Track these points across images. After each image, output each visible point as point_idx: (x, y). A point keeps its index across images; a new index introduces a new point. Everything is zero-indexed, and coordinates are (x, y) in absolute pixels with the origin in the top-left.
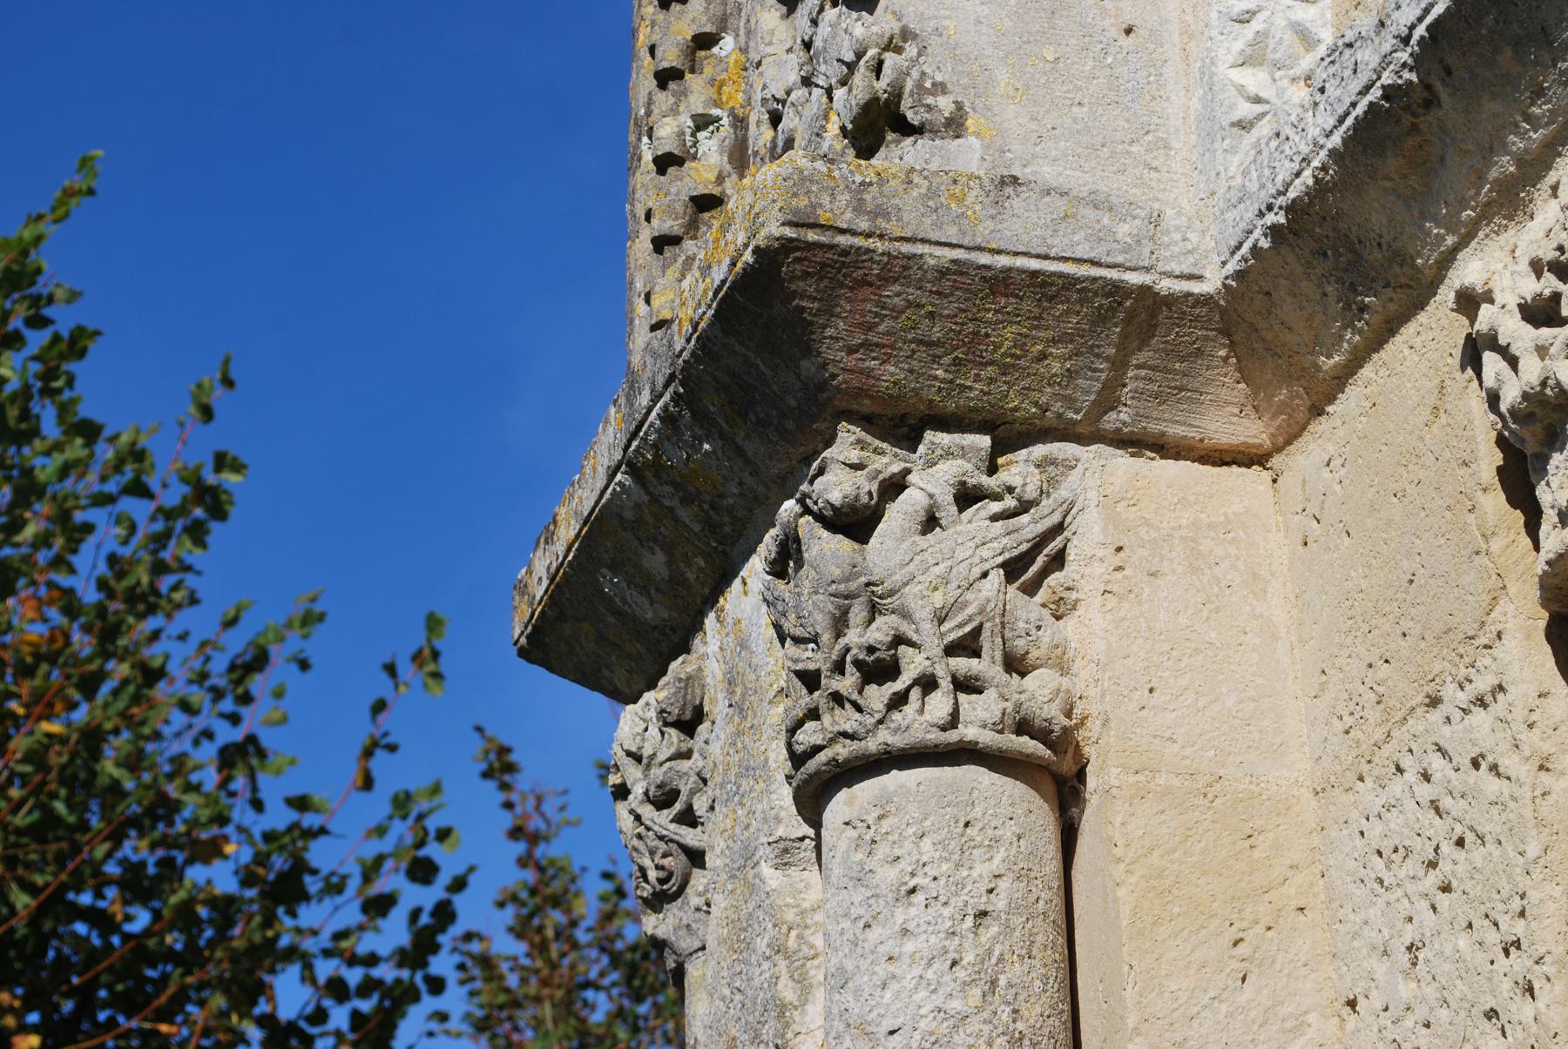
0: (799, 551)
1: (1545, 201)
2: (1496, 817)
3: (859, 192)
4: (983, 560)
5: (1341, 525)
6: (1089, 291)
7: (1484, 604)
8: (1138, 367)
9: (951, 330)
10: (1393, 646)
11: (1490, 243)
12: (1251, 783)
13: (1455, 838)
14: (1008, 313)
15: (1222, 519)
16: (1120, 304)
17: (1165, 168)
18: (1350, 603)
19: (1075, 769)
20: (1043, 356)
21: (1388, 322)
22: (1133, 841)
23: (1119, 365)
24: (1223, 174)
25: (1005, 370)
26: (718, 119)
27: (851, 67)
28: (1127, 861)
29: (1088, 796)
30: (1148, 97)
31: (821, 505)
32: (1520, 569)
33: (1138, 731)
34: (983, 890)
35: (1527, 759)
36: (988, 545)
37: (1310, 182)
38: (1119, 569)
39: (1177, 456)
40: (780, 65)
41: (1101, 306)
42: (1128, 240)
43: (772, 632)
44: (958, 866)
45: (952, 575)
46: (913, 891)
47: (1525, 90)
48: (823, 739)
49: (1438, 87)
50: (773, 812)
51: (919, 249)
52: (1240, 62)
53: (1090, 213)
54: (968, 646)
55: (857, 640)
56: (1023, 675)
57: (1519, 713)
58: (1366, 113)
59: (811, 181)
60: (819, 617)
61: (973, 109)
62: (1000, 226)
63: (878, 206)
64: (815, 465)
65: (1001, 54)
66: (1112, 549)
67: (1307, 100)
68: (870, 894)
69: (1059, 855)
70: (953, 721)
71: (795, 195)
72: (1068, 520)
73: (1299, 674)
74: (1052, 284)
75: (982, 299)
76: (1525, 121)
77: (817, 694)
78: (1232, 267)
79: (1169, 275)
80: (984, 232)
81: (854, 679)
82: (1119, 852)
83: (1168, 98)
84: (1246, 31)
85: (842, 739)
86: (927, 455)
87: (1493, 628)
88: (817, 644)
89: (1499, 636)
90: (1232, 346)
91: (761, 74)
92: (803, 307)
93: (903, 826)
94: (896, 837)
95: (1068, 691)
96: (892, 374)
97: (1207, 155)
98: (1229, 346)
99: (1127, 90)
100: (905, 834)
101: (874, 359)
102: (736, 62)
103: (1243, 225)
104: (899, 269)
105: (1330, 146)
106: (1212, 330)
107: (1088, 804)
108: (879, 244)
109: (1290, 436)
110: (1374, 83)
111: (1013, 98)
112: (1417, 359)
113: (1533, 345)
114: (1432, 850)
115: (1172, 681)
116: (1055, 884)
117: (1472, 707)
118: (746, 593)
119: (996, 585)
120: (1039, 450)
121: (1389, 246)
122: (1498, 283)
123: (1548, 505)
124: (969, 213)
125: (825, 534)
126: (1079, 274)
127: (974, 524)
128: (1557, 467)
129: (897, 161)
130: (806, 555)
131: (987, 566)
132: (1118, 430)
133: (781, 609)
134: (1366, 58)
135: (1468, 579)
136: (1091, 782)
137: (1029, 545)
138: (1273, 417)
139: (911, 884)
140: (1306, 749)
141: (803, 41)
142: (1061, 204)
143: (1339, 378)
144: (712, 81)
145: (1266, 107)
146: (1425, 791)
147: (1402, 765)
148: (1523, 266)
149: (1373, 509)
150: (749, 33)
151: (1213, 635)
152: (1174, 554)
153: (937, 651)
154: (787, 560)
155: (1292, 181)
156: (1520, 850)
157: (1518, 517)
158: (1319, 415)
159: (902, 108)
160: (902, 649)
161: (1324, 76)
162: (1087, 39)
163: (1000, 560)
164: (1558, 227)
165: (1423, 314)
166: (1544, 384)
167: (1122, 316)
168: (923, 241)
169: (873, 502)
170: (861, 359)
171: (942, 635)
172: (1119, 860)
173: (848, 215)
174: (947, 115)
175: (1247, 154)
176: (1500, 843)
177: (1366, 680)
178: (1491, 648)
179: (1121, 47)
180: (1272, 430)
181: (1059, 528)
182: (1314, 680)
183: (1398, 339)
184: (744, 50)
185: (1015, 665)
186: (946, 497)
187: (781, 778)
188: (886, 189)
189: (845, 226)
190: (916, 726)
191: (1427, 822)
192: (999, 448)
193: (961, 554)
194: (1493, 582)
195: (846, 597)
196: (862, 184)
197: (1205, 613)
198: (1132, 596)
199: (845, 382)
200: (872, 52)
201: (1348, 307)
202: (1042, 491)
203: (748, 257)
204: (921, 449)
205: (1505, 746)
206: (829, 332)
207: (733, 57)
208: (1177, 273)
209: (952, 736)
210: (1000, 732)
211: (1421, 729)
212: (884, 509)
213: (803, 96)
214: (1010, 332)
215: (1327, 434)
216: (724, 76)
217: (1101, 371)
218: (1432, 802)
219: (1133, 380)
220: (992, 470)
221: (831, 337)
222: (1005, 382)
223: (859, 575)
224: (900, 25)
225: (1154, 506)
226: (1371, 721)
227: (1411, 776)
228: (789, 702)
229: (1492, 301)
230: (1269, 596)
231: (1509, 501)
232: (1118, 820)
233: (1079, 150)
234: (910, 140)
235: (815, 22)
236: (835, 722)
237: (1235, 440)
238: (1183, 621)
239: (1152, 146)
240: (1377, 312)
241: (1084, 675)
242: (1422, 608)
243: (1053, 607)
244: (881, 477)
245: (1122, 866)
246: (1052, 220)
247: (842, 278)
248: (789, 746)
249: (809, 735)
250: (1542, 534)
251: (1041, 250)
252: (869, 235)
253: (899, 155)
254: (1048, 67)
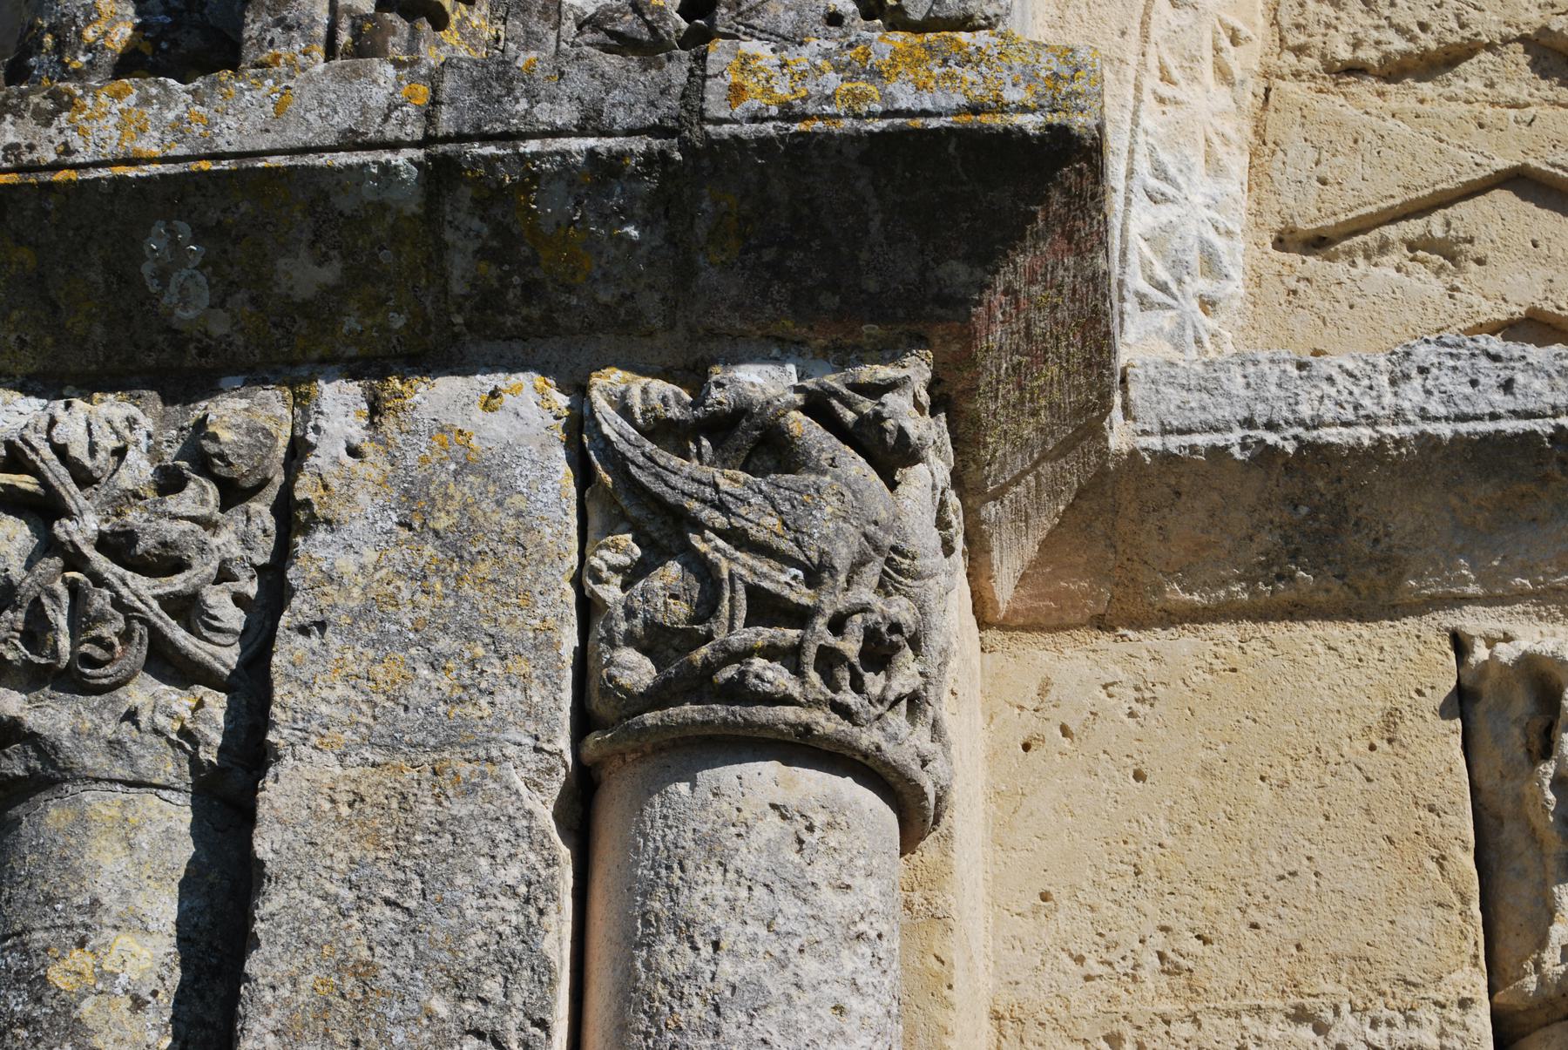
11: (1525, 622)
52: (1147, 236)
58: (1516, 435)
143: (1170, 614)
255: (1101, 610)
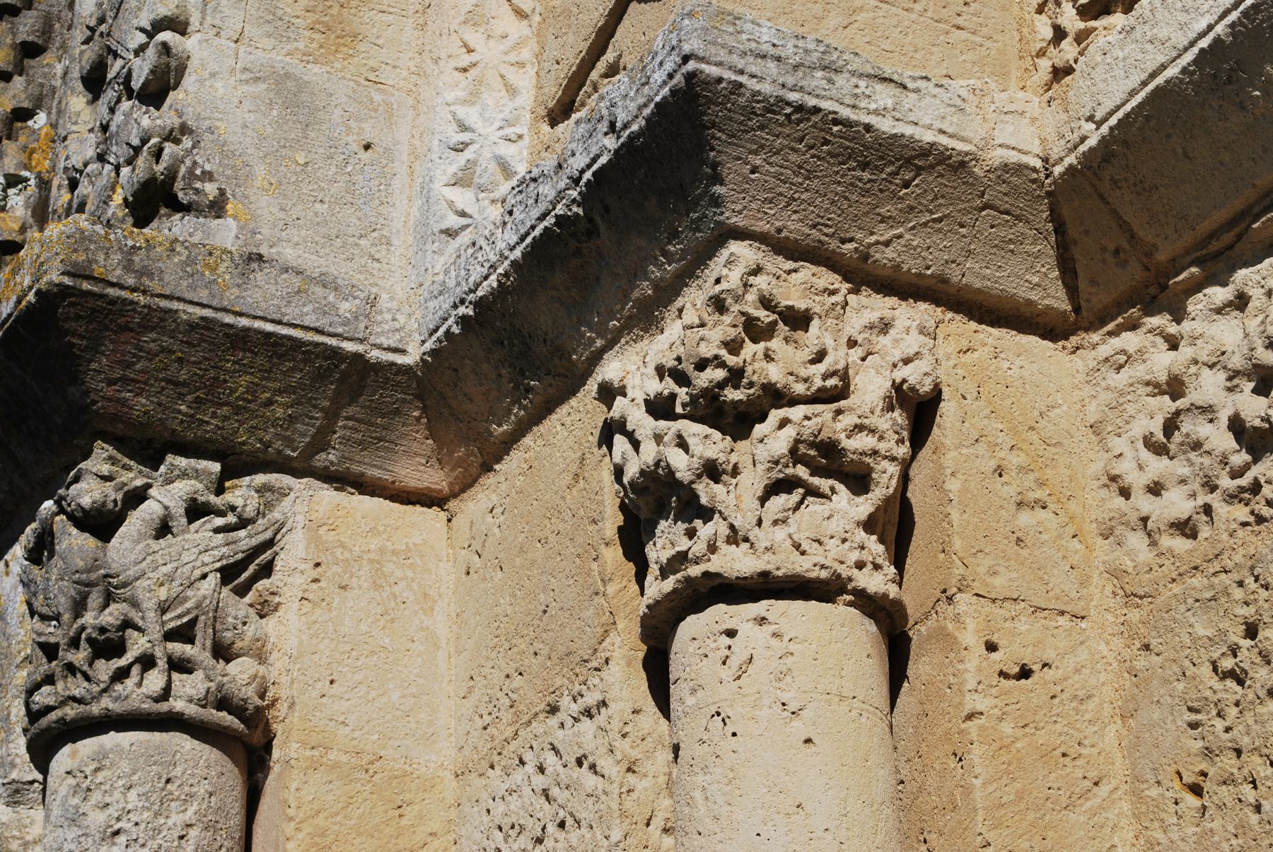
0: (53, 544)
1: (673, 320)
2: (591, 807)
3: (130, 254)
4: (204, 564)
5: (497, 561)
6: (313, 353)
7: (598, 635)
8: (347, 418)
9: (196, 374)
10: (526, 662)
11: (629, 349)
12: (405, 763)
13: (558, 821)
14: (244, 365)
15: (404, 547)
16: (336, 366)
17: (386, 261)
18: (497, 624)
19: (263, 741)
20: (270, 402)
21: (547, 402)
22: (303, 804)
23: (332, 416)
24: (430, 270)
25: (237, 410)
26: (27, 180)
27: (137, 150)
28: (297, 820)
29: (272, 764)
30: (377, 202)
31: (73, 507)
32: (628, 609)
33: (318, 714)
34: (176, 836)
35: (619, 762)
36: (210, 552)
37: (495, 285)
38: (316, 581)
39: (373, 494)
40: (82, 141)
41: (321, 367)
42: (348, 315)
43: (25, 608)
44: (157, 814)
45: (177, 575)
46: (117, 833)
47: (664, 232)
48: (56, 701)
49: (599, 221)
50: (9, 759)
51: (175, 305)
53: (319, 291)
54: (184, 634)
55: (92, 621)
56: (228, 661)
57: (616, 725)
58: (541, 234)
59: (90, 241)
60: (63, 600)
61: (234, 196)
62: (244, 294)
63: (145, 267)
64: (72, 474)
65: (261, 154)
66: (311, 564)
67: (498, 221)
68: (81, 833)
69: (243, 812)
70: (166, 694)
71: (75, 251)
72: (278, 537)
73: (453, 678)
74: (282, 345)
75: (223, 351)
76: (662, 256)
77: (54, 663)
78: (429, 345)
79: (379, 347)
80: (230, 296)
81: (86, 653)
82: (291, 812)
83: (394, 204)
84: (459, 158)
85: (71, 703)
86: (166, 474)
87: (603, 654)
88: (59, 622)
89: (607, 661)
90: (424, 409)
91: (66, 147)
92: (74, 344)
93: (115, 779)
94: (108, 787)
95: (263, 677)
96: (143, 405)
97: (420, 253)
98: (422, 409)
99: (361, 194)
100: (115, 785)
101: (129, 391)
102: (47, 134)
103: (440, 313)
104: (158, 320)
105: (512, 257)
106: (409, 394)
107: (271, 771)
108: (141, 298)
109: (464, 486)
110: (550, 212)
111: (267, 190)
112: (566, 434)
113: (652, 433)
114: (540, 829)
115: (349, 676)
116: (237, 835)
117: (581, 717)
118: (7, 574)
119: (213, 586)
120: (260, 479)
121: (552, 343)
122: (631, 381)
123: (653, 560)
124: (220, 280)
125: (74, 531)
126: (306, 339)
127: (200, 534)
128: (663, 532)
129: (166, 231)
130: (57, 547)
131: (207, 569)
132: (326, 468)
133: (33, 589)
134: (546, 192)
135: (588, 614)
136: (276, 753)
137: (244, 555)
138: (453, 469)
139: (116, 827)
140: (453, 739)
141: (101, 124)
142: (296, 281)
144: (24, 149)
145: (468, 221)
146: (539, 781)
147: (524, 759)
148: (651, 370)
149: (522, 550)
150: (59, 112)
151: (387, 641)
152: (362, 573)
153: (157, 636)
154: (41, 551)
155: (481, 282)
156: (606, 834)
157: (631, 568)
158: (489, 471)
159: (175, 189)
160: (129, 631)
161: (513, 202)
162: (332, 150)
163: (218, 565)
164: (678, 342)
165: (574, 399)
166: (657, 464)
167: (337, 376)
168: (179, 299)
169: (117, 509)
170: (118, 391)
171: (163, 623)
172: (291, 819)
173: (118, 272)
174: (211, 198)
175: (450, 256)
176: (592, 828)
177: (504, 688)
178: (600, 670)
179: (360, 160)
180: (450, 479)
181: (270, 543)
182: (464, 684)
183: (554, 416)
184: (54, 126)
185: (223, 652)
186: (178, 510)
187: (19, 730)
188: (152, 254)
189: (115, 281)
190: (134, 696)
191: (538, 807)
192: (227, 474)
193: (186, 557)
194: (606, 618)
195: (87, 585)
196: (133, 247)
197: (382, 623)
198: (324, 604)
199: (103, 407)
200: (154, 141)
201: (516, 387)
202: (258, 513)
203: (31, 297)
204: (162, 469)
205: (603, 750)
206: (94, 366)
207: (45, 130)
208: (385, 346)
209: (163, 707)
210: (204, 707)
211: (541, 731)
212: (126, 515)
213: (97, 169)
214: (244, 380)
215: (493, 487)
216: (35, 145)
217: (317, 419)
218: (544, 790)
219: (342, 429)
220: (220, 491)
221: (95, 370)
222: (236, 421)
223: (99, 568)
224: (180, 121)
225: (349, 532)
226: (504, 721)
227: (530, 768)
228: (31, 668)
229: (625, 395)
230: (436, 612)
231: (625, 554)
232: (294, 785)
233: (317, 239)
234: (178, 216)
235: (112, 110)
236: (66, 688)
237: (420, 485)
238: (363, 627)
239: (377, 241)
240: (539, 394)
241: (278, 665)
242: (551, 634)
243: (259, 607)
244: (126, 489)
245: (292, 824)
246: (287, 293)
247: (108, 323)
248: (27, 705)
249: (44, 697)
250: (646, 584)
251: (276, 317)
252: (133, 290)
253: (175, 227)
254: (299, 169)
255: (481, 460)
